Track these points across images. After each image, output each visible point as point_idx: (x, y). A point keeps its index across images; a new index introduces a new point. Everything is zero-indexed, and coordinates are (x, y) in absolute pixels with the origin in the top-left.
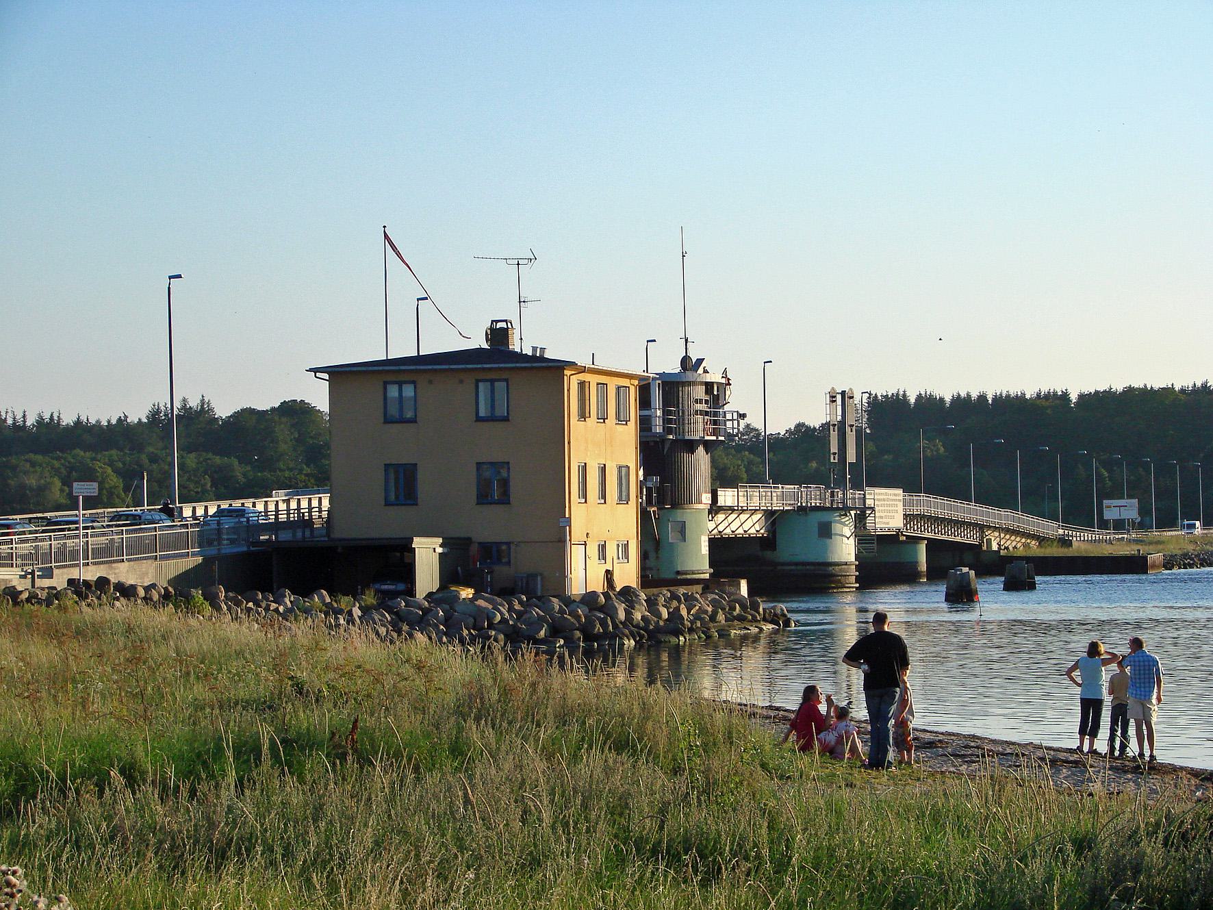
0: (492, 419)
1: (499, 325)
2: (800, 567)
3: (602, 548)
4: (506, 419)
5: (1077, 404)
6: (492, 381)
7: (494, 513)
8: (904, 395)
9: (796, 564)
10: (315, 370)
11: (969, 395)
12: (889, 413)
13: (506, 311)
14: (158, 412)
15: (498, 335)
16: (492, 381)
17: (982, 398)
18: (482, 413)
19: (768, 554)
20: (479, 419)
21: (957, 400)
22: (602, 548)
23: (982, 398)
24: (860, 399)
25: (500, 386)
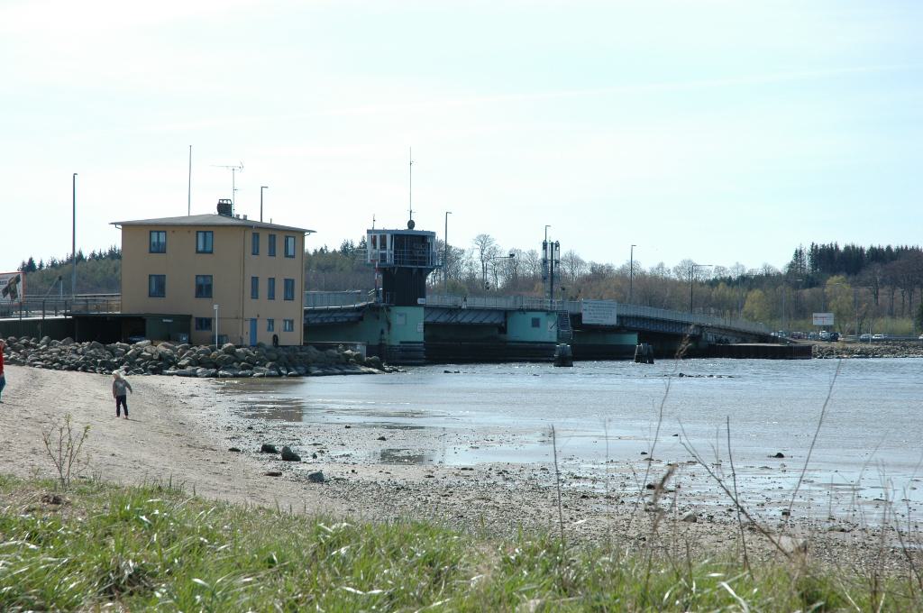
0: (204, 252)
1: (225, 202)
2: (543, 345)
3: (271, 322)
4: (211, 252)
5: (868, 252)
6: (158, 232)
7: (204, 301)
8: (836, 246)
9: (518, 342)
10: (115, 224)
11: (889, 248)
12: (829, 260)
13: (226, 195)
14: (347, 245)
15: (225, 208)
16: (158, 232)
17: (889, 248)
18: (201, 247)
19: (502, 336)
20: (198, 252)
21: (872, 249)
22: (271, 322)
23: (889, 248)
24: (807, 249)
25: (209, 235)
